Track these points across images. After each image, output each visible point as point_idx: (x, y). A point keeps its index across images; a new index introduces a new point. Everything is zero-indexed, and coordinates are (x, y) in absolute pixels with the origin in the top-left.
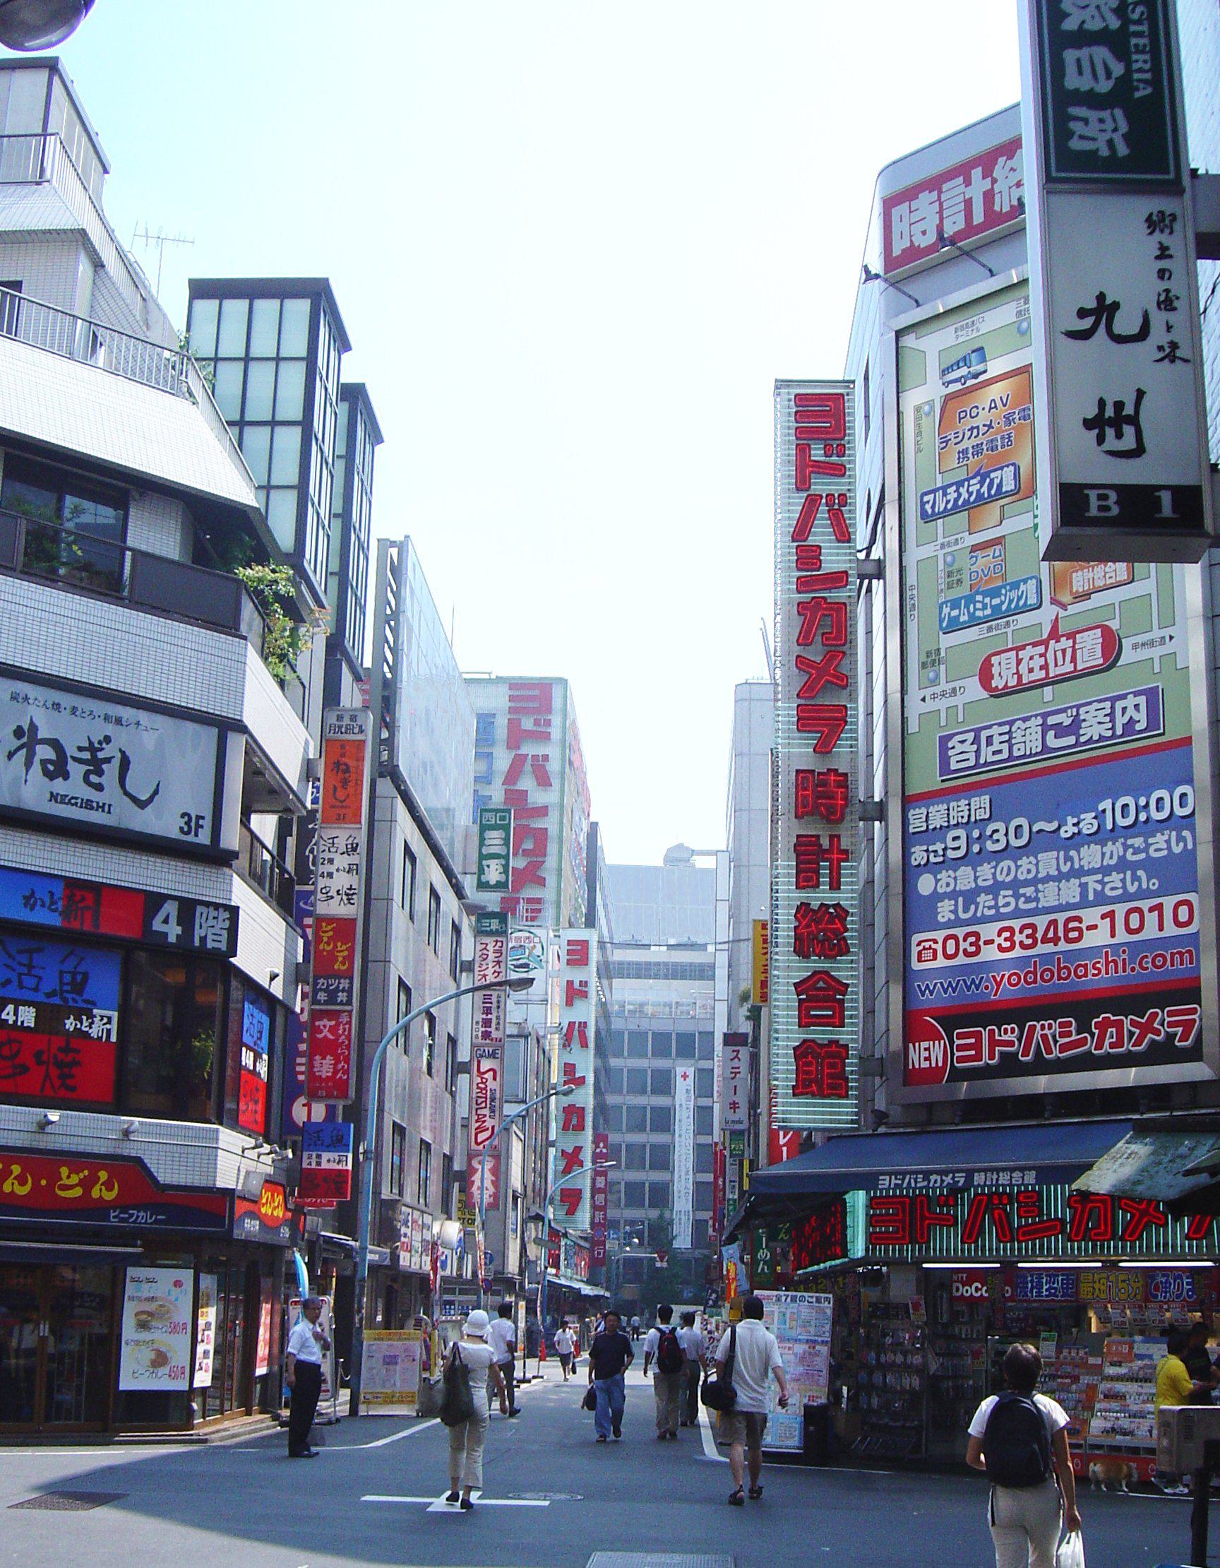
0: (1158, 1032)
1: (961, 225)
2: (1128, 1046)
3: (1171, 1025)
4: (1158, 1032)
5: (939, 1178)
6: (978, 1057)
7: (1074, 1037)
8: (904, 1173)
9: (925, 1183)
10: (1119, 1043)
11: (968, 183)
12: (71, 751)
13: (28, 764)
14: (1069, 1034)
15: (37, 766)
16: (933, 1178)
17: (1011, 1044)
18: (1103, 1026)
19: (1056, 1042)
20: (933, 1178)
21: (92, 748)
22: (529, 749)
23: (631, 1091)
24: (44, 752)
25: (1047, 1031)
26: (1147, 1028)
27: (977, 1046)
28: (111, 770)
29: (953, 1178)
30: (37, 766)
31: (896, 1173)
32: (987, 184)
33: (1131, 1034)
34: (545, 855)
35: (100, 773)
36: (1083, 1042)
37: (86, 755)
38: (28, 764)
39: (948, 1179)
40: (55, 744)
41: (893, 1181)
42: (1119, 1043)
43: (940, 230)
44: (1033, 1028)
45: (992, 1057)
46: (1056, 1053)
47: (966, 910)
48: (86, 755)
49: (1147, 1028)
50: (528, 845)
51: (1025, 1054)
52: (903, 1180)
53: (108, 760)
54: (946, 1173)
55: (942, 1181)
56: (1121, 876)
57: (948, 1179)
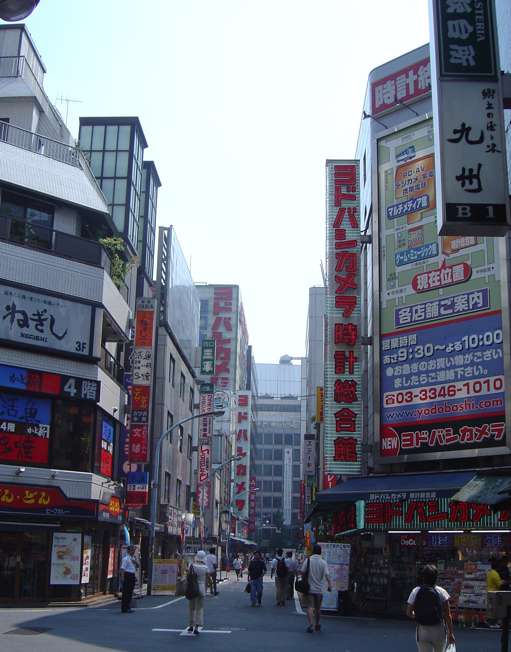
0: (487, 434)
1: (404, 94)
2: (475, 440)
3: (493, 431)
4: (487, 434)
5: (395, 495)
6: (412, 444)
7: (452, 436)
8: (380, 493)
9: (389, 497)
10: (471, 438)
11: (407, 77)
12: (30, 315)
13: (12, 321)
14: (450, 435)
15: (15, 322)
16: (393, 495)
17: (425, 439)
18: (464, 432)
19: (444, 438)
20: (393, 495)
21: (39, 315)
22: (223, 315)
23: (266, 458)
24: (19, 316)
25: (440, 433)
26: (483, 432)
27: (411, 440)
28: (47, 324)
29: (401, 495)
30: (15, 322)
31: (377, 493)
32: (415, 77)
33: (476, 435)
34: (229, 360)
35: (42, 325)
36: (456, 438)
37: (36, 317)
38: (12, 321)
39: (399, 496)
40: (23, 313)
41: (376, 496)
42: (471, 438)
43: (396, 97)
44: (435, 432)
45: (417, 444)
46: (444, 442)
47: (406, 383)
48: (36, 317)
49: (483, 432)
50: (222, 355)
51: (431, 443)
52: (380, 496)
53: (45, 320)
54: (398, 493)
55: (397, 496)
56: (472, 368)
57: (399, 496)
